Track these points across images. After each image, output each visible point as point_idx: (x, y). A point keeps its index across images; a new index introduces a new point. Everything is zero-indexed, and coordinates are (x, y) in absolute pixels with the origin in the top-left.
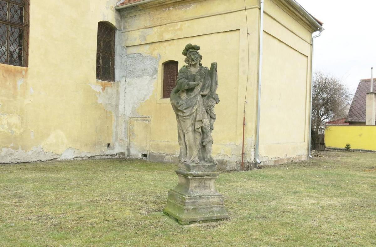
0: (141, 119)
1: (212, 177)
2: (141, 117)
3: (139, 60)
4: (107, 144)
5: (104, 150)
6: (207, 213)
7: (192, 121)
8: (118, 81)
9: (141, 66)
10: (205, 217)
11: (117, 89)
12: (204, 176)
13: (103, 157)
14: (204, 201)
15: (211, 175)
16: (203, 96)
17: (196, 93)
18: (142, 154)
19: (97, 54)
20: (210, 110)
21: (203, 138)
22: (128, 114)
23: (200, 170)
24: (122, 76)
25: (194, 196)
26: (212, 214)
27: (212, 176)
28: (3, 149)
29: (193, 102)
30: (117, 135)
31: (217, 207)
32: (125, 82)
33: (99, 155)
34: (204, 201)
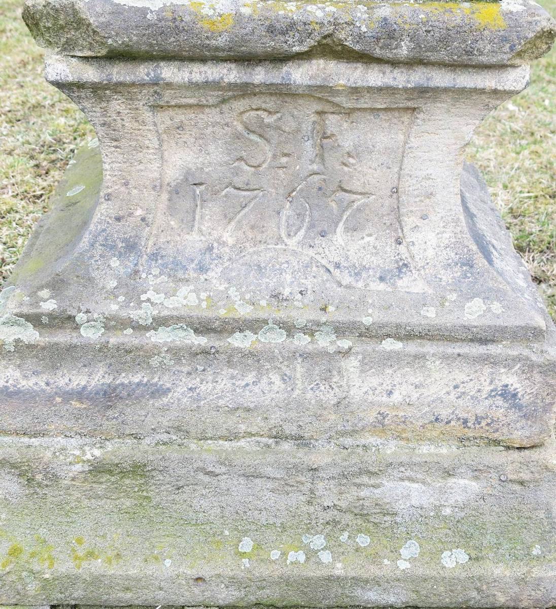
1: (417, 77)
6: (293, 528)
10: (264, 571)
12: (280, 59)
14: (268, 389)
15: (404, 50)
25: (113, 324)
26: (363, 540)
27: (411, 63)
31: (448, 473)
34: (268, 389)
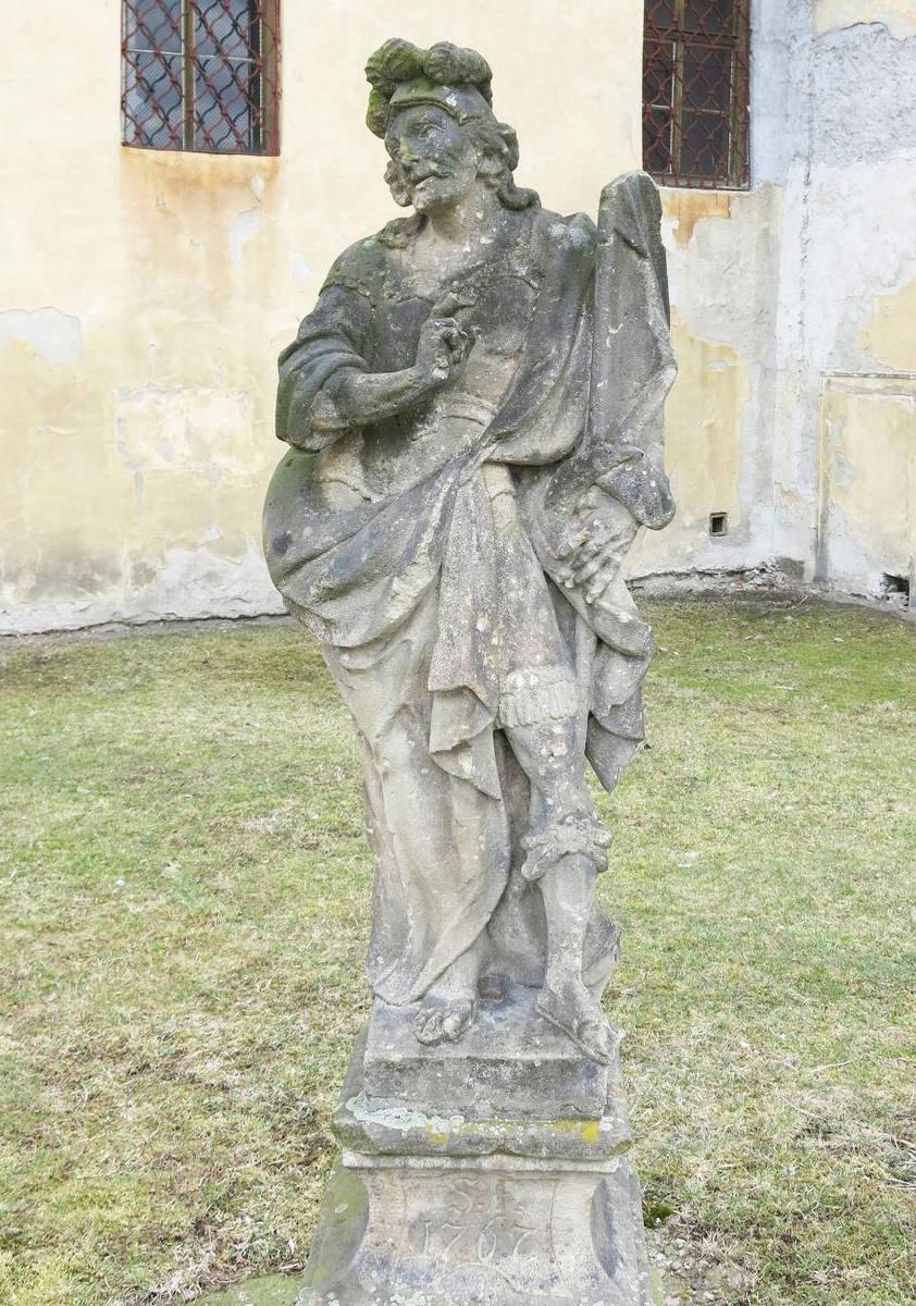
0: (880, 384)
2: (879, 376)
3: (872, 60)
4: (708, 515)
5: (690, 549)
7: (398, 690)
8: (768, 186)
9: (885, 92)
11: (765, 225)
13: (684, 584)
16: (520, 472)
17: (434, 460)
18: (889, 577)
19: (649, 47)
20: (582, 585)
21: (518, 827)
22: (819, 356)
23: (453, 1096)
24: (793, 153)
28: (171, 555)
29: (396, 535)
30: (765, 464)
32: (807, 183)
33: (665, 574)
